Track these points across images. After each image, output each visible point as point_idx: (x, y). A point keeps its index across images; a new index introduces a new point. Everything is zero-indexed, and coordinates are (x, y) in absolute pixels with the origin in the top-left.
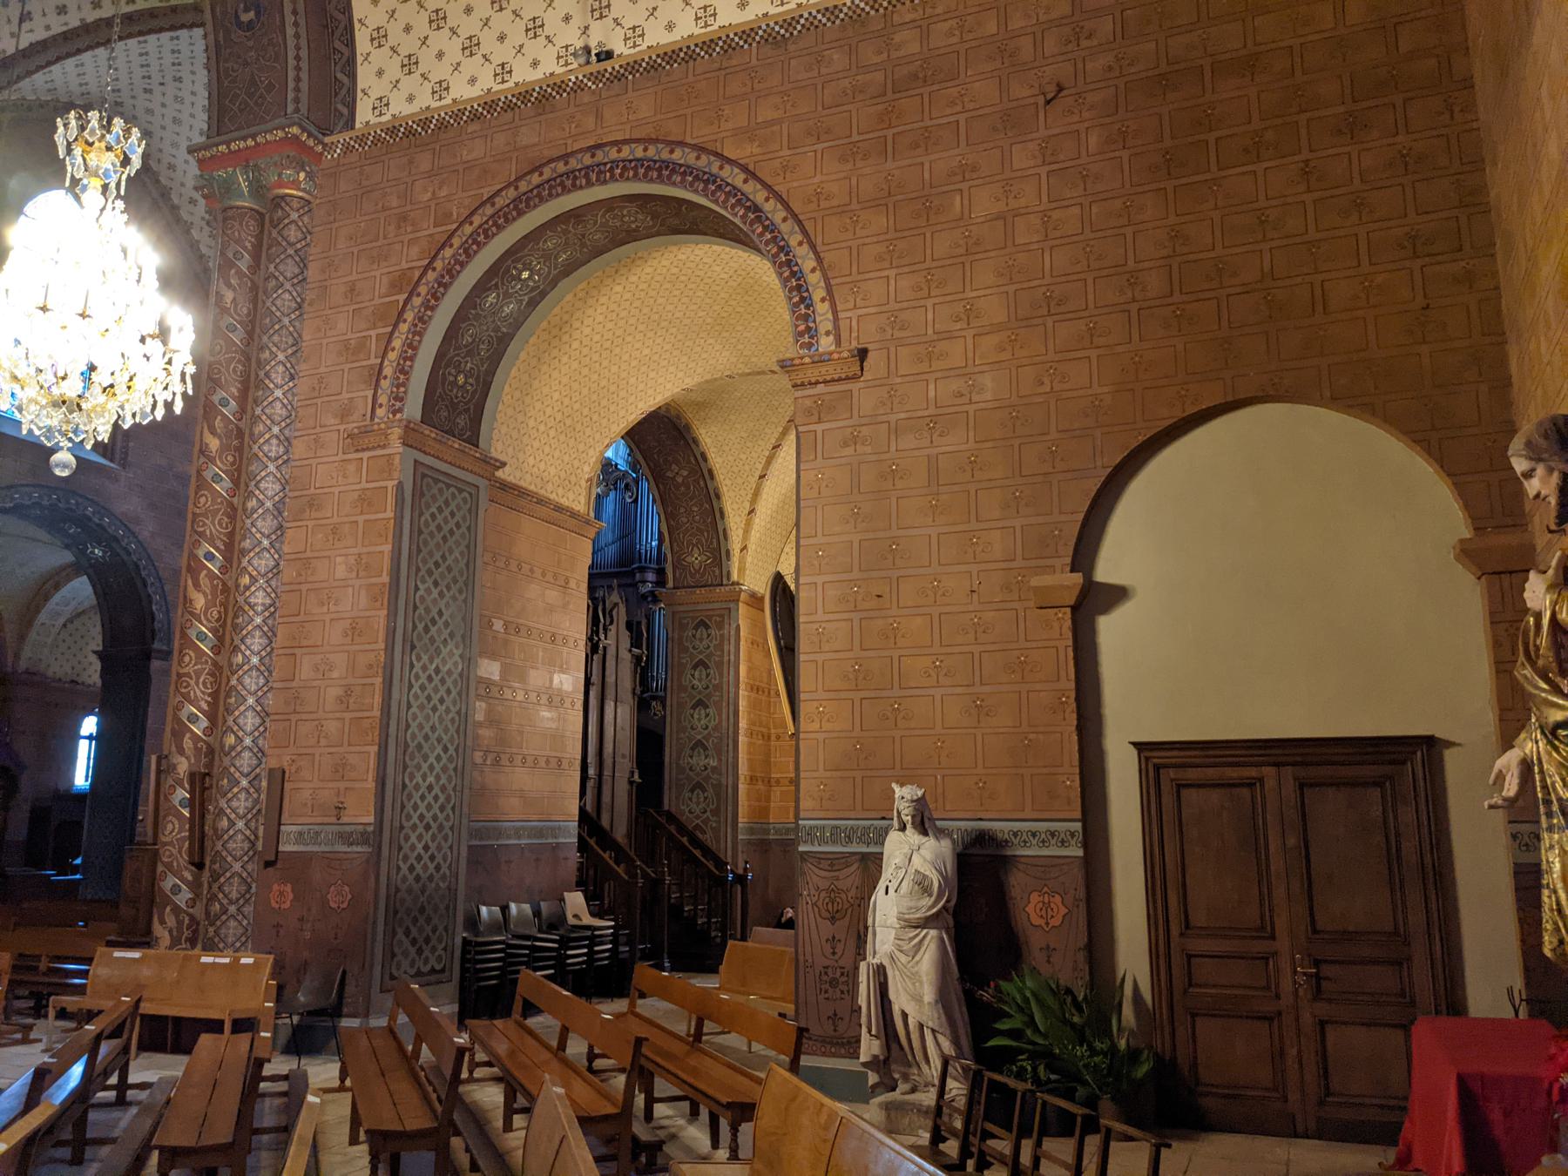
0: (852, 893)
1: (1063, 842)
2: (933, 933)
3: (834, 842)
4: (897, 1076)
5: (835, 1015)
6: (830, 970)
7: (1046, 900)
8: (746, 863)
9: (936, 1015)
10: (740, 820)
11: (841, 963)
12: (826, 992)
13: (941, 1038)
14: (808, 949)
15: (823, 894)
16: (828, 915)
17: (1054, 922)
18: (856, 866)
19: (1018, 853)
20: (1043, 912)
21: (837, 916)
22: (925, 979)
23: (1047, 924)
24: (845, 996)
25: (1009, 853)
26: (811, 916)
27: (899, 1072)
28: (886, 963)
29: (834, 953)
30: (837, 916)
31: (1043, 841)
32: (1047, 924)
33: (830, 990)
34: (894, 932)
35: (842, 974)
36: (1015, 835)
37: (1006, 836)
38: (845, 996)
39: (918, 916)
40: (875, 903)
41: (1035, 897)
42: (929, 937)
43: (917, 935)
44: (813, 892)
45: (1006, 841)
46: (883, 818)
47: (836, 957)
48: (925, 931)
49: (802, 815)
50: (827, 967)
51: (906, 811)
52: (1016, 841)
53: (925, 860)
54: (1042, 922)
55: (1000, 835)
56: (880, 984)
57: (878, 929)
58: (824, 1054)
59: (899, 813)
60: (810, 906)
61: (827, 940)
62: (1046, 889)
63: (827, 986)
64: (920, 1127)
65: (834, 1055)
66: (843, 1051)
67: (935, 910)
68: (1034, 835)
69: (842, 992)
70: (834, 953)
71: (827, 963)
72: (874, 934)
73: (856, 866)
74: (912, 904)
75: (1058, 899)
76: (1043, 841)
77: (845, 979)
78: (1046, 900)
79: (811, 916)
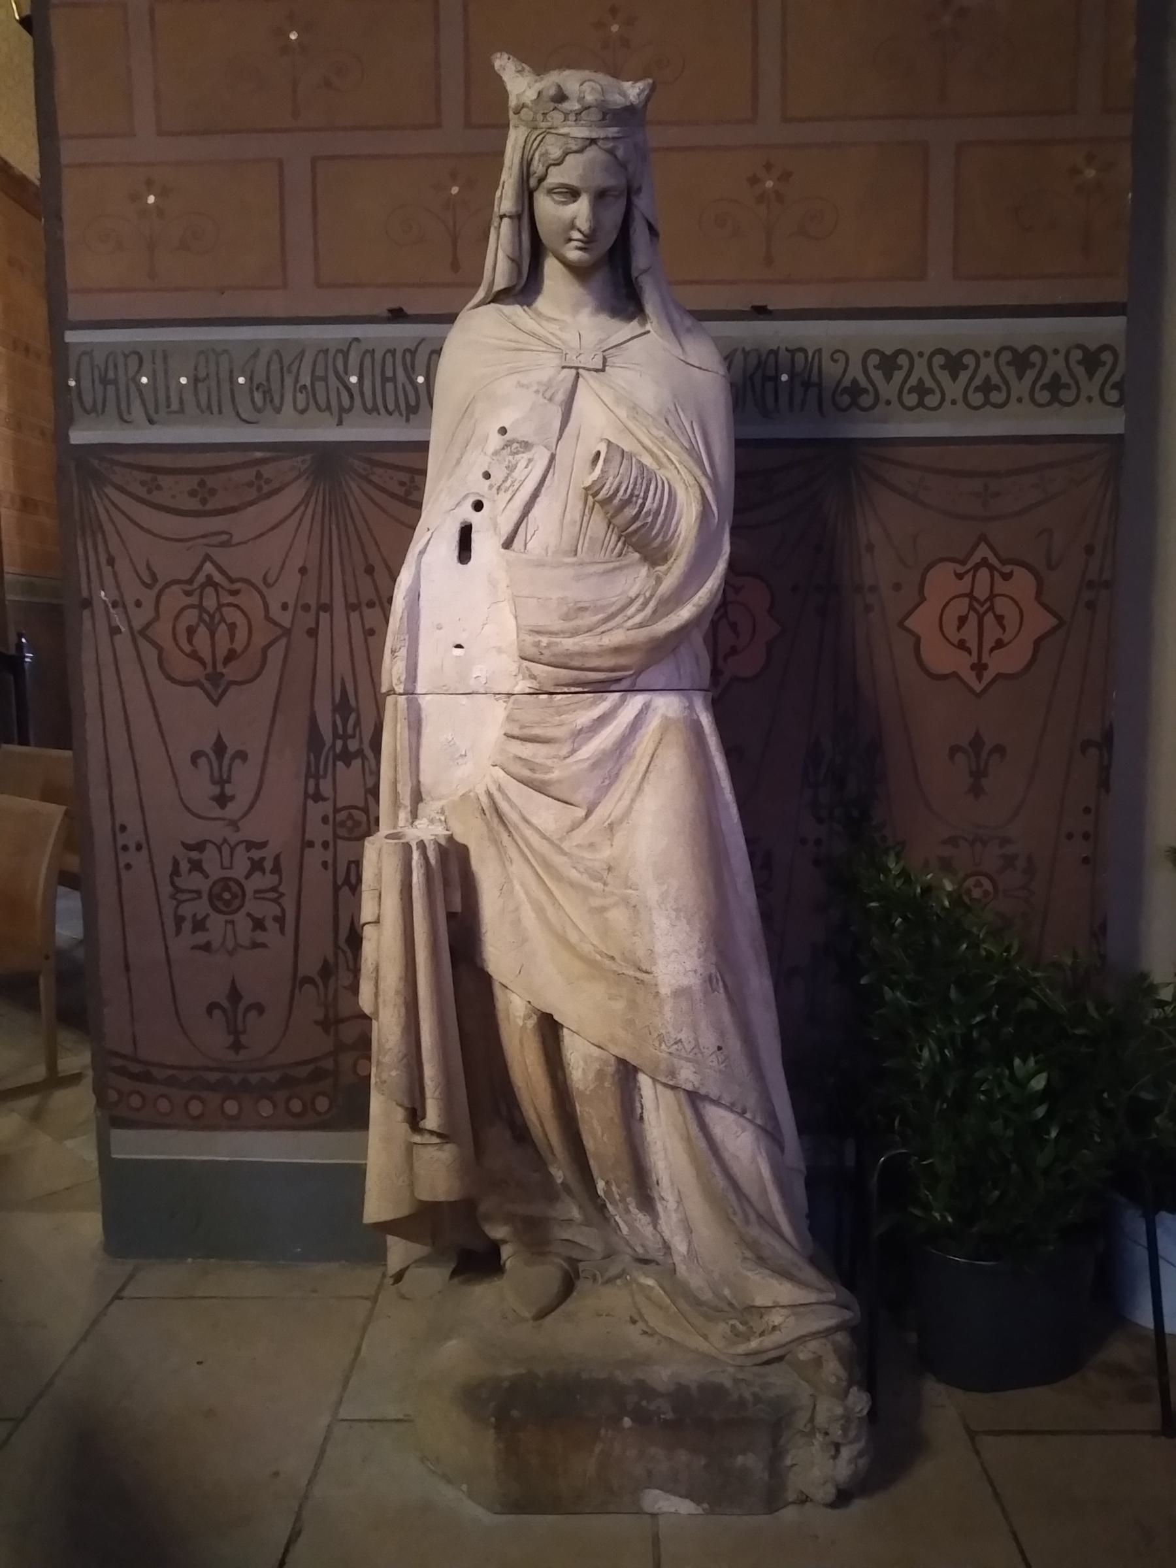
0: (287, 589)
1: (1055, 386)
2: (667, 706)
3: (210, 410)
4: (498, 1232)
5: (235, 995)
6: (210, 857)
7: (982, 592)
8: (20, 636)
9: (709, 1040)
10: (6, 568)
11: (250, 830)
12: (199, 925)
13: (722, 1122)
14: (124, 786)
15: (174, 599)
16: (196, 672)
17: (997, 663)
18: (294, 494)
19: (892, 430)
20: (969, 633)
21: (231, 672)
22: (653, 893)
23: (979, 668)
24: (271, 934)
25: (863, 429)
26: (130, 672)
27: (509, 1219)
28: (470, 833)
29: (222, 800)
30: (231, 672)
31: (987, 388)
32: (979, 668)
33: (216, 921)
34: (499, 710)
35: (257, 866)
36: (888, 363)
37: (855, 372)
38: (271, 934)
39: (617, 637)
40: (415, 596)
41: (942, 582)
42: (653, 723)
43: (602, 721)
44: (133, 591)
45: (855, 391)
46: (397, 315)
47: (233, 810)
48: (637, 701)
49: (77, 308)
50: (200, 847)
51: (568, 173)
52: (888, 390)
53: (634, 409)
54: (961, 663)
55: (832, 370)
56: (451, 916)
57: (427, 703)
58: (200, 1123)
59: (527, 193)
60: (123, 642)
61: (195, 757)
62: (983, 551)
63: (202, 907)
64: (650, 1481)
65: (234, 1124)
66: (266, 1109)
67: (685, 613)
68: (954, 365)
69: (259, 924)
70: (222, 800)
71: (196, 831)
72: (416, 725)
73: (294, 494)
74: (583, 593)
75: (1022, 583)
76: (987, 388)
77: (269, 880)
78: (982, 592)
79: (130, 672)
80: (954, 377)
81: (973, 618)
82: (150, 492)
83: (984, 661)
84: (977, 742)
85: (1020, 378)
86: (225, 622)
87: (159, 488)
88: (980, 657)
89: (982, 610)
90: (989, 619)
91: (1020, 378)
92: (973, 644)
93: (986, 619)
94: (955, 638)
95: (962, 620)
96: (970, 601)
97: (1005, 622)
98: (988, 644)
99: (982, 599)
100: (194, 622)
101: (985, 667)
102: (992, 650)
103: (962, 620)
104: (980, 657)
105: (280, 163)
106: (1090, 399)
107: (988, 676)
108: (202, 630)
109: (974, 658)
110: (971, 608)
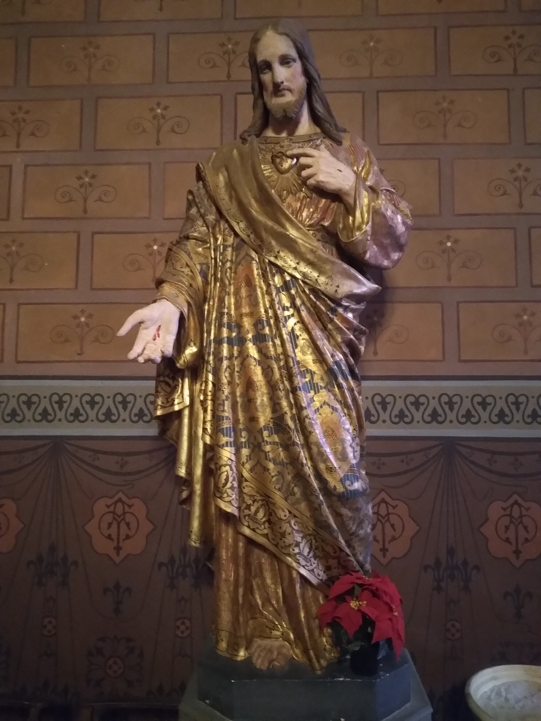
20: (113, 531)
23: (517, 552)
80: (92, 408)
81: (512, 527)
82: (379, 468)
83: (386, 547)
84: (117, 586)
85: (435, 409)
86: (390, 523)
87: (98, 459)
88: (517, 547)
89: (119, 520)
90: (388, 526)
91: (435, 409)
92: (513, 540)
93: (121, 524)
94: (106, 533)
95: (507, 528)
96: (511, 519)
97: (395, 527)
98: (122, 537)
99: (119, 514)
100: (507, 523)
101: (387, 550)
102: (124, 540)
103: (110, 525)
104: (517, 547)
105: (19, 304)
106: (518, 422)
107: (123, 554)
108: (512, 527)
109: (115, 544)
110: (114, 519)
